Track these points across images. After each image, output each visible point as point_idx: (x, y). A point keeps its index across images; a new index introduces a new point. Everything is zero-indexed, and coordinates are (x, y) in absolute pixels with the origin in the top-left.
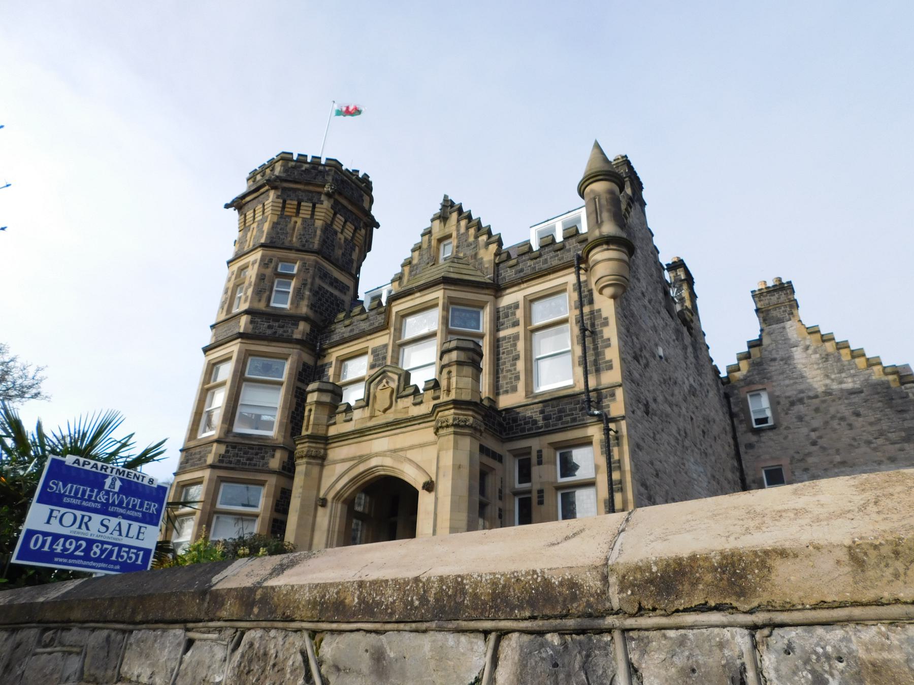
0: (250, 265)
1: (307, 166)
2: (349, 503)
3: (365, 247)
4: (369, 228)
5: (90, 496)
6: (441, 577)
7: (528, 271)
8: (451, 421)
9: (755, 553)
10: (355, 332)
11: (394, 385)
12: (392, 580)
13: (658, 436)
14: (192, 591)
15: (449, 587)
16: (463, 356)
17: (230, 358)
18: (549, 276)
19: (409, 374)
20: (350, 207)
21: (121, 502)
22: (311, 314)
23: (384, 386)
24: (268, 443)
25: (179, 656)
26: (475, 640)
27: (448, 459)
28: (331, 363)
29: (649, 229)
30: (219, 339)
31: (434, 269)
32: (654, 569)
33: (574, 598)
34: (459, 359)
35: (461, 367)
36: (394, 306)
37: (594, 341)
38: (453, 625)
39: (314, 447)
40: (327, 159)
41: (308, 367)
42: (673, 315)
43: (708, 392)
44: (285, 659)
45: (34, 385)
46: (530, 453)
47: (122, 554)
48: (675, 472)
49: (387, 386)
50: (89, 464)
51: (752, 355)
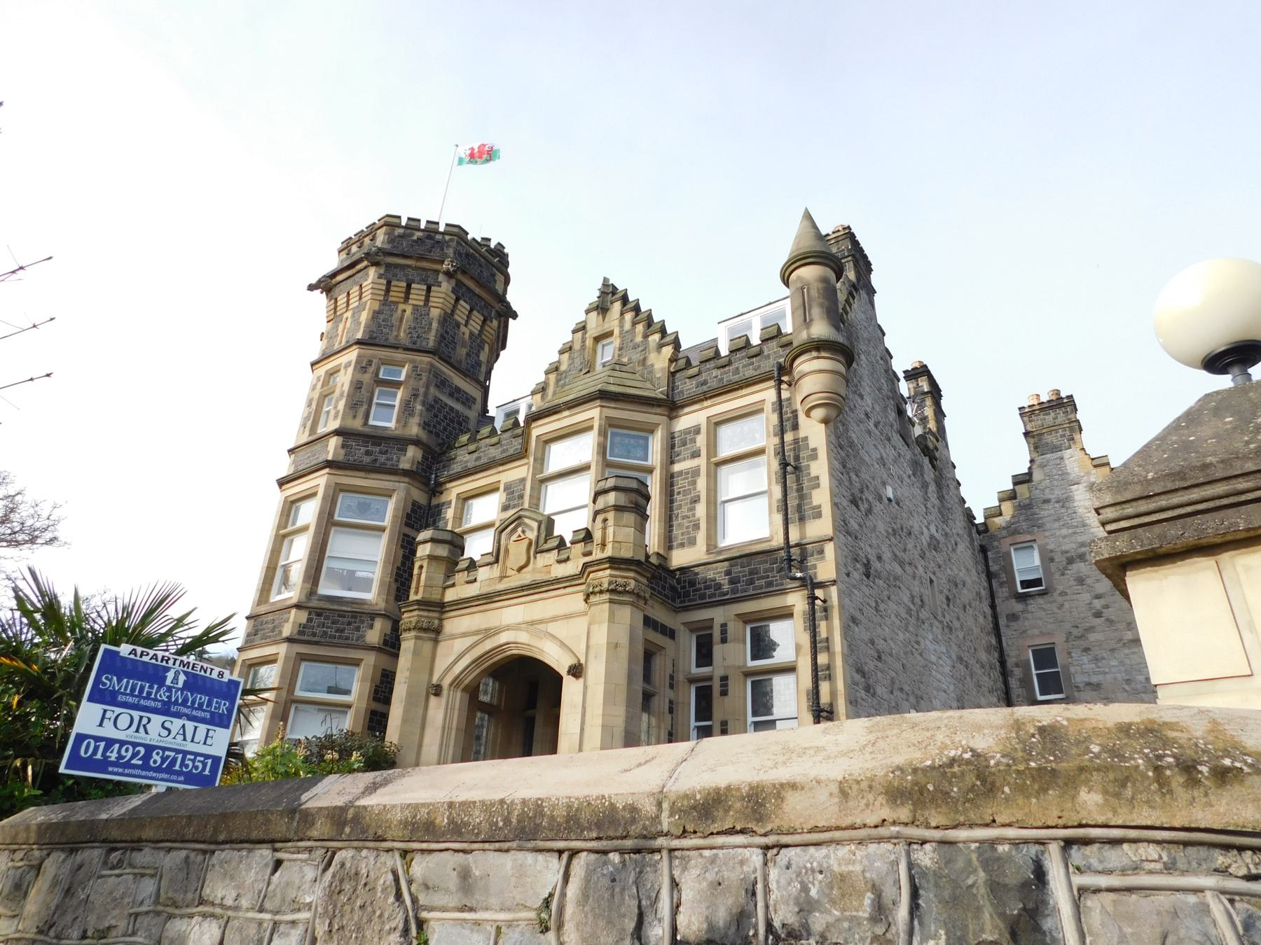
0: (342, 369)
1: (420, 234)
2: (472, 692)
3: (498, 343)
4: (502, 319)
5: (149, 693)
6: (524, 799)
7: (713, 384)
8: (605, 586)
9: (774, 785)
10: (482, 461)
11: (532, 535)
12: (480, 801)
13: (882, 607)
14: (281, 809)
15: (530, 809)
16: (622, 499)
17: (314, 495)
18: (740, 391)
19: (553, 521)
20: (477, 290)
21: (185, 700)
22: (423, 436)
23: (520, 536)
24: (366, 609)
25: (267, 877)
26: (550, 859)
27: (601, 635)
28: (450, 502)
29: (879, 326)
30: (301, 468)
31: (588, 378)
32: (698, 797)
33: (633, 821)
34: (618, 504)
35: (620, 514)
36: (534, 428)
37: (798, 479)
38: (531, 844)
39: (427, 617)
40: (447, 225)
41: (420, 507)
42: (910, 442)
43: (956, 544)
44: (376, 879)
45: (49, 526)
46: (711, 627)
47: (187, 762)
48: (906, 653)
49: (523, 537)
50: (148, 654)
51: (1018, 495)
